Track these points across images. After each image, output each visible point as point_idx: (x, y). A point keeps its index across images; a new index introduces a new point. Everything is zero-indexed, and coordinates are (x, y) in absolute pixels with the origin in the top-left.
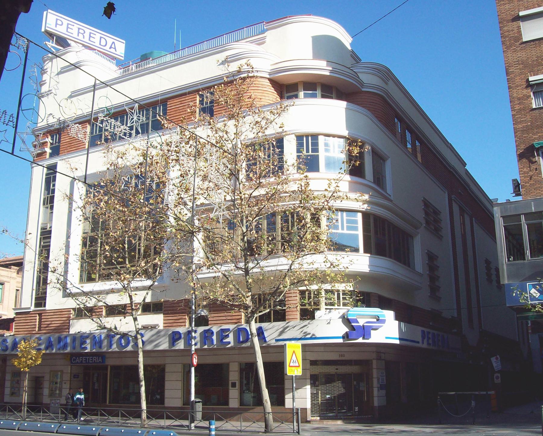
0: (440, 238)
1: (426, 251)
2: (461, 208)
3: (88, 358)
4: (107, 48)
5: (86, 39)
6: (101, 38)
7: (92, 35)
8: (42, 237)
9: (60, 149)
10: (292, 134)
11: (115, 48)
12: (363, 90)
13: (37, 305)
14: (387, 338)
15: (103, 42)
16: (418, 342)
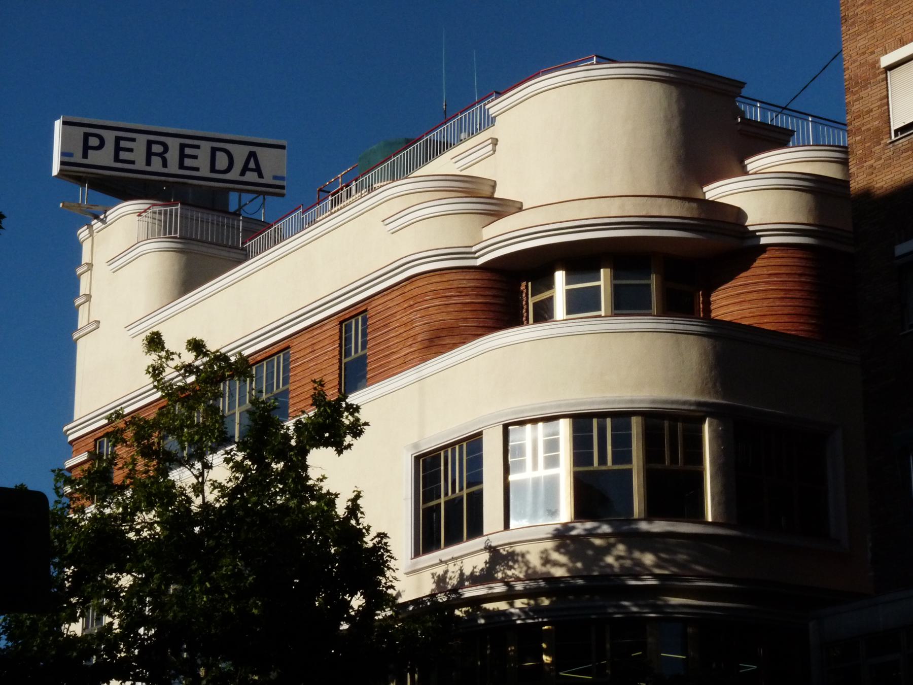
4: (234, 175)
6: (214, 151)
15: (222, 161)
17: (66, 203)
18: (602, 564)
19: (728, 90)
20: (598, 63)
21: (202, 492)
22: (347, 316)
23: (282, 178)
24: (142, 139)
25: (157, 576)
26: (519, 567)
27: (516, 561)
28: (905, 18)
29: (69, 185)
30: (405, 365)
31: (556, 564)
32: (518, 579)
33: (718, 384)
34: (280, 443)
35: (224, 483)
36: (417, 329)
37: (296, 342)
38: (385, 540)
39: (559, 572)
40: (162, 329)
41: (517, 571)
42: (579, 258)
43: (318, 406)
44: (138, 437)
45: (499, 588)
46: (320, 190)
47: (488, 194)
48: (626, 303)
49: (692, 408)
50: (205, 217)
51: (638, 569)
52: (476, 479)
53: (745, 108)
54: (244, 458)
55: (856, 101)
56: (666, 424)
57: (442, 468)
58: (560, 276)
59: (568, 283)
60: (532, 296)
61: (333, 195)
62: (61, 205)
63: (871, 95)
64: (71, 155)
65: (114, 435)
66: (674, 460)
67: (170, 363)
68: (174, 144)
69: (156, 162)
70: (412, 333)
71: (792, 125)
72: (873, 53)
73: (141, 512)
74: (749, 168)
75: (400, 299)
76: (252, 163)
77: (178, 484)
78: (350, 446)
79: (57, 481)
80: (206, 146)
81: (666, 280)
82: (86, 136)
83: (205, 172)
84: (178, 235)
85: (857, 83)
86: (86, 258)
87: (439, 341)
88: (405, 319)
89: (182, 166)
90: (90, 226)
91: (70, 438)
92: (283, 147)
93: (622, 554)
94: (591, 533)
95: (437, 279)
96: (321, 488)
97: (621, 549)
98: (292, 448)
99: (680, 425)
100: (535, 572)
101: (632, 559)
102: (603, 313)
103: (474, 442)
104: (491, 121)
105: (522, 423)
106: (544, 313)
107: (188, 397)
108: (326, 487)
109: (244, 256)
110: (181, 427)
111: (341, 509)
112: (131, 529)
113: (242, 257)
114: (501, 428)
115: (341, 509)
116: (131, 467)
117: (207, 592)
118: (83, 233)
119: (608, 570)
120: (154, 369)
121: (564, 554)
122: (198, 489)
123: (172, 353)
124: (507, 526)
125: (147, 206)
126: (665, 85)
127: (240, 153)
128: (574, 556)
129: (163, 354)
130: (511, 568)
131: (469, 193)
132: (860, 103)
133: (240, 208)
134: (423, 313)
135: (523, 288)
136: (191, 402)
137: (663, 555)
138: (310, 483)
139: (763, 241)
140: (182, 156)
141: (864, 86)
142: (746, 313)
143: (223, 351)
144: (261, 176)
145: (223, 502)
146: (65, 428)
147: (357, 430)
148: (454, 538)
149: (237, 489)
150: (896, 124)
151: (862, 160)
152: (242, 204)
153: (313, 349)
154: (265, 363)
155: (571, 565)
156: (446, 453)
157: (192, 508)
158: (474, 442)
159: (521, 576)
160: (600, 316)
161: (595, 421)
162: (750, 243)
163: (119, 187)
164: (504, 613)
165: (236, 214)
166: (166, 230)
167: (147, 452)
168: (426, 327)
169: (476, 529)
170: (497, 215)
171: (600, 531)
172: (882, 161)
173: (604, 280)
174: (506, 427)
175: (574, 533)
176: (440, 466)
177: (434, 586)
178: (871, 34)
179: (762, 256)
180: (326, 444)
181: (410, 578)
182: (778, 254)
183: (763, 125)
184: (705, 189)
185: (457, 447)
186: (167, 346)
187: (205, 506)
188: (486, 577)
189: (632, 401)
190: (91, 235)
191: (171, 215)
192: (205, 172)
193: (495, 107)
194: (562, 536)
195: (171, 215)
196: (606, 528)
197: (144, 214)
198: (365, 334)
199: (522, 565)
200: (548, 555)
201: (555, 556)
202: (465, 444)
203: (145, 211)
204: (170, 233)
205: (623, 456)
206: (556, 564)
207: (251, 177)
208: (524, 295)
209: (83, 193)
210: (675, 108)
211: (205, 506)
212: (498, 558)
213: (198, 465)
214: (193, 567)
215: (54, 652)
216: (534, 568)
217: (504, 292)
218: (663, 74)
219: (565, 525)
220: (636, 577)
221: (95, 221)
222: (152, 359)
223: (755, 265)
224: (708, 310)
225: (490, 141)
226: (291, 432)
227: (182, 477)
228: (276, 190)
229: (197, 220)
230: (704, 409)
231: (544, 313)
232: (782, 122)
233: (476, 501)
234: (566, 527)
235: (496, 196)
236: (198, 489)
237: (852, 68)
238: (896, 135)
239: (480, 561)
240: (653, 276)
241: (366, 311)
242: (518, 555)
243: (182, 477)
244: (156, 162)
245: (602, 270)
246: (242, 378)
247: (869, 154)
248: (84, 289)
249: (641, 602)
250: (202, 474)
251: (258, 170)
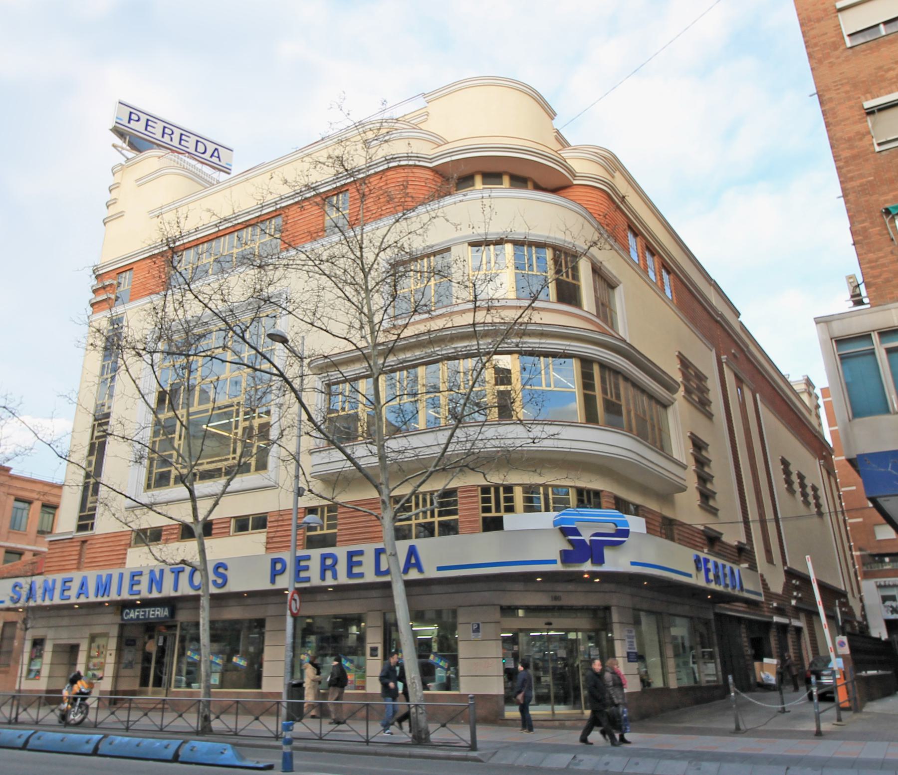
0: (709, 416)
1: (689, 434)
2: (737, 376)
3: (147, 610)
4: (207, 156)
5: (175, 142)
6: (197, 141)
7: (183, 137)
8: (96, 423)
10: (464, 242)
11: (218, 157)
12: (575, 182)
13: (81, 528)
14: (440, 569)
15: (201, 148)
16: (690, 576)
127: (211, 148)
207: (215, 159)
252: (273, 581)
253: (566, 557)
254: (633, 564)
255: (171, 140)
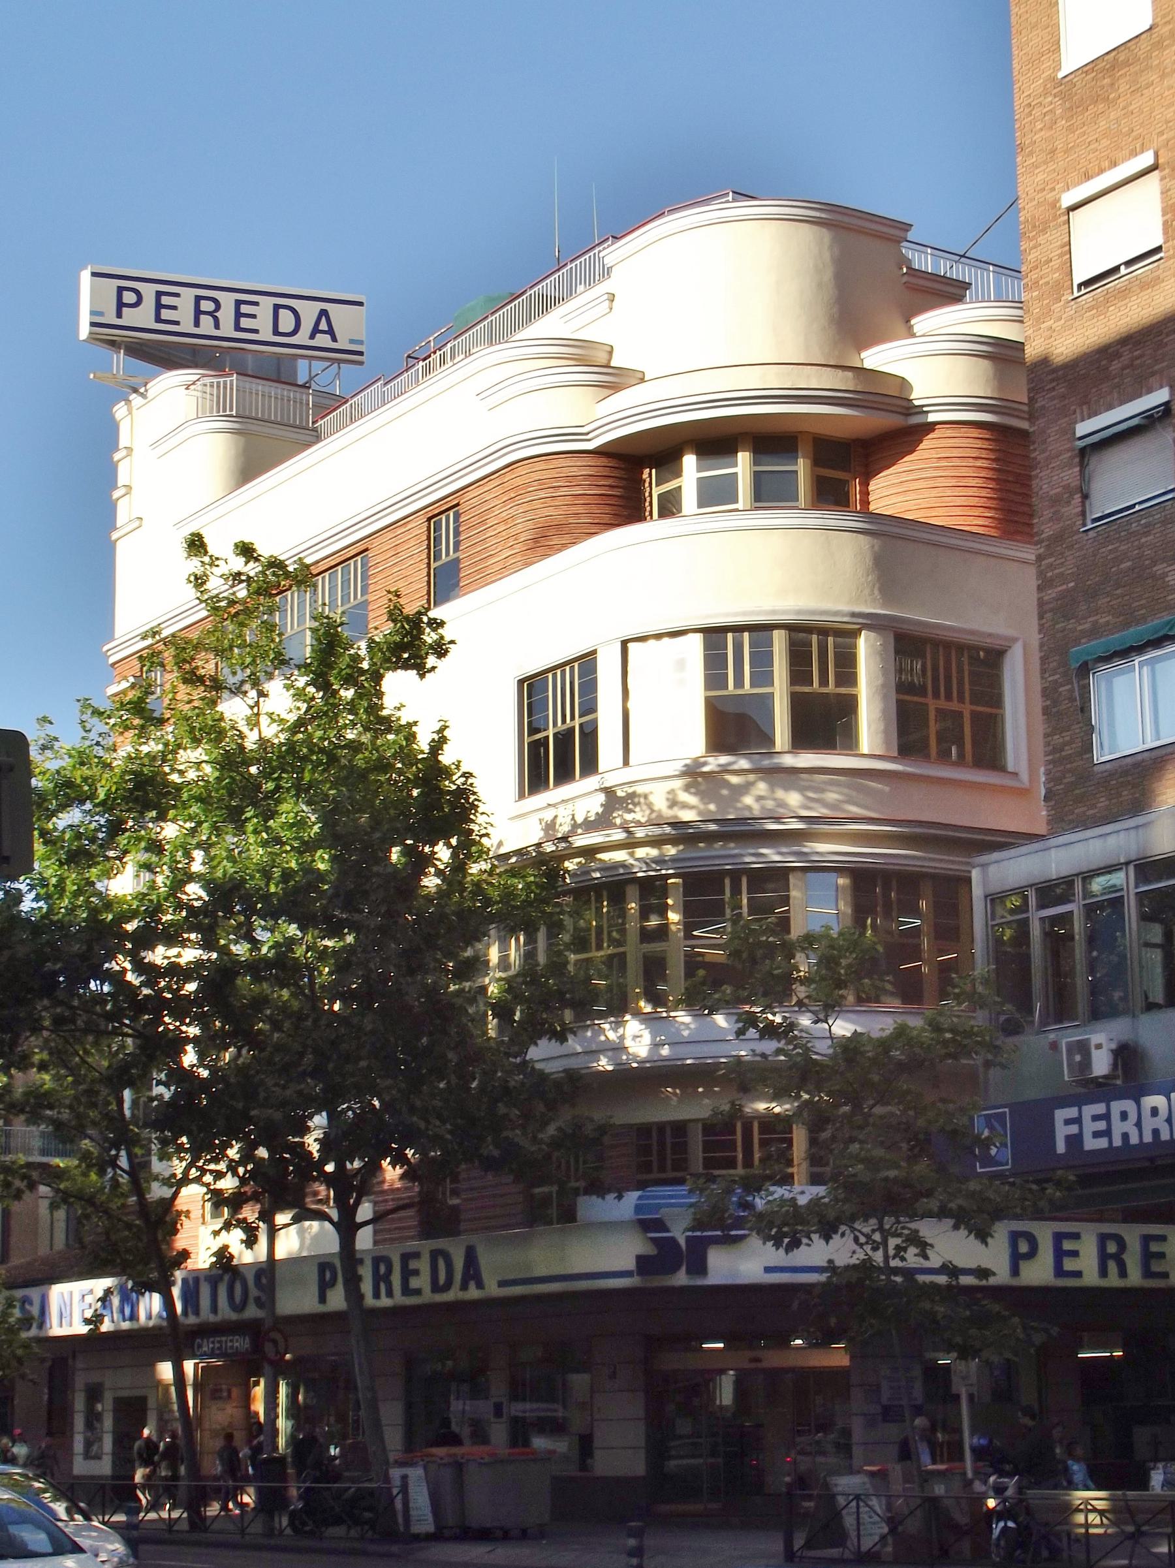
4: (302, 338)
6: (277, 307)
9: (459, 570)
15: (286, 321)
17: (99, 374)
18: (739, 805)
19: (892, 232)
20: (734, 200)
21: (257, 724)
22: (436, 512)
23: (361, 342)
24: (189, 294)
25: (205, 825)
26: (642, 810)
27: (635, 805)
28: (1092, 147)
29: (104, 351)
30: (506, 570)
31: (685, 806)
32: (639, 824)
33: (876, 592)
34: (348, 666)
35: (284, 716)
36: (520, 526)
37: (376, 542)
38: (470, 781)
39: (688, 816)
40: (203, 532)
41: (640, 815)
42: (714, 440)
43: (394, 621)
44: (180, 662)
45: (618, 835)
46: (409, 357)
47: (604, 362)
48: (768, 493)
49: (845, 619)
50: (267, 389)
51: (781, 810)
52: (590, 707)
53: (913, 255)
54: (307, 685)
55: (1035, 247)
56: (814, 638)
57: (967, 686)
58: (689, 461)
59: (699, 470)
60: (657, 485)
61: (424, 359)
62: (92, 376)
63: (1050, 241)
64: (101, 314)
65: (150, 659)
66: (739, 682)
67: (214, 569)
68: (227, 301)
69: (206, 321)
70: (513, 531)
71: (970, 277)
72: (1053, 189)
73: (185, 749)
74: (916, 329)
75: (499, 490)
76: (324, 324)
77: (227, 716)
78: (434, 668)
79: (83, 713)
80: (267, 303)
81: (817, 461)
82: (121, 290)
83: (266, 334)
84: (234, 413)
85: (1034, 227)
86: (123, 441)
87: (546, 540)
88: (504, 514)
89: (238, 328)
90: (128, 402)
91: (112, 660)
92: (360, 304)
93: (762, 793)
94: (725, 770)
95: (542, 466)
96: (399, 719)
97: (762, 787)
98: (362, 672)
99: (830, 640)
100: (660, 816)
101: (775, 799)
102: (740, 506)
103: (587, 662)
104: (607, 272)
105: (642, 639)
106: (670, 507)
107: (237, 614)
108: (405, 717)
109: (316, 437)
110: (231, 648)
111: (423, 742)
112: (173, 770)
113: (314, 439)
114: (619, 644)
115: (423, 742)
116: (170, 696)
117: (265, 844)
118: (120, 411)
119: (747, 814)
120: (196, 578)
121: (695, 794)
122: (254, 721)
123: (217, 559)
124: (626, 762)
125: (196, 377)
126: (815, 228)
127: (309, 312)
128: (704, 795)
129: (206, 559)
130: (631, 811)
131: (582, 361)
132: (1037, 252)
133: (311, 378)
134: (525, 507)
135: (645, 475)
136: (241, 617)
137: (811, 795)
138: (385, 713)
139: (932, 418)
140: (238, 315)
141: (1042, 231)
142: (911, 505)
143: (282, 558)
144: (334, 339)
145: (283, 737)
146: (105, 648)
147: (441, 649)
148: (565, 775)
149: (300, 724)
150: (1078, 278)
151: (1039, 321)
152: (313, 374)
153: (396, 550)
154: (339, 568)
155: (702, 807)
156: (555, 676)
157: (246, 744)
158: (587, 662)
159: (643, 820)
160: (737, 510)
161: (730, 635)
162: (916, 420)
163: (161, 354)
164: (623, 865)
165: (305, 386)
166: (220, 407)
167: (192, 678)
168: (530, 525)
169: (590, 765)
170: (615, 388)
171: (736, 767)
172: (1063, 321)
173: (743, 464)
174: (624, 644)
175: (706, 769)
176: (547, 691)
177: (542, 834)
178: (1052, 166)
179: (930, 436)
180: (406, 666)
181: (510, 821)
182: (949, 433)
183: (934, 277)
184: (863, 355)
185: (568, 668)
186: (211, 551)
187: (263, 742)
188: (602, 822)
189: (774, 612)
190: (130, 413)
191: (225, 388)
192: (266, 334)
193: (612, 254)
194: (693, 774)
195: (225, 388)
196: (744, 764)
197: (192, 387)
198: (457, 533)
199: (645, 807)
200: (675, 795)
201: (684, 797)
202: (576, 665)
203: (194, 383)
204: (225, 411)
205: (763, 676)
206: (685, 806)
207: (323, 340)
208: (647, 485)
209: (119, 360)
210: (827, 255)
211: (263, 742)
212: (613, 800)
213: (253, 694)
214: (248, 815)
215: (84, 915)
216: (660, 811)
217: (628, 478)
218: (817, 214)
219: (696, 760)
220: (778, 819)
221: (134, 395)
222: (194, 565)
223: (921, 446)
224: (866, 503)
225: (606, 297)
226: (363, 652)
227: (233, 709)
228: (353, 355)
229: (257, 394)
230: (860, 621)
231: (670, 507)
232: (964, 274)
233: (590, 736)
234: (697, 763)
235: (612, 364)
236: (254, 721)
237: (1028, 209)
238: (1079, 289)
239: (594, 805)
240: (801, 461)
241: (458, 505)
242: (639, 796)
243: (233, 709)
244: (206, 321)
245: (740, 454)
246: (303, 588)
247: (1047, 313)
248: (122, 479)
249: (784, 850)
250: (257, 704)
251: (331, 332)
252: (322, 1299)
253: (644, 1263)
254: (768, 1270)
255: (217, 326)
